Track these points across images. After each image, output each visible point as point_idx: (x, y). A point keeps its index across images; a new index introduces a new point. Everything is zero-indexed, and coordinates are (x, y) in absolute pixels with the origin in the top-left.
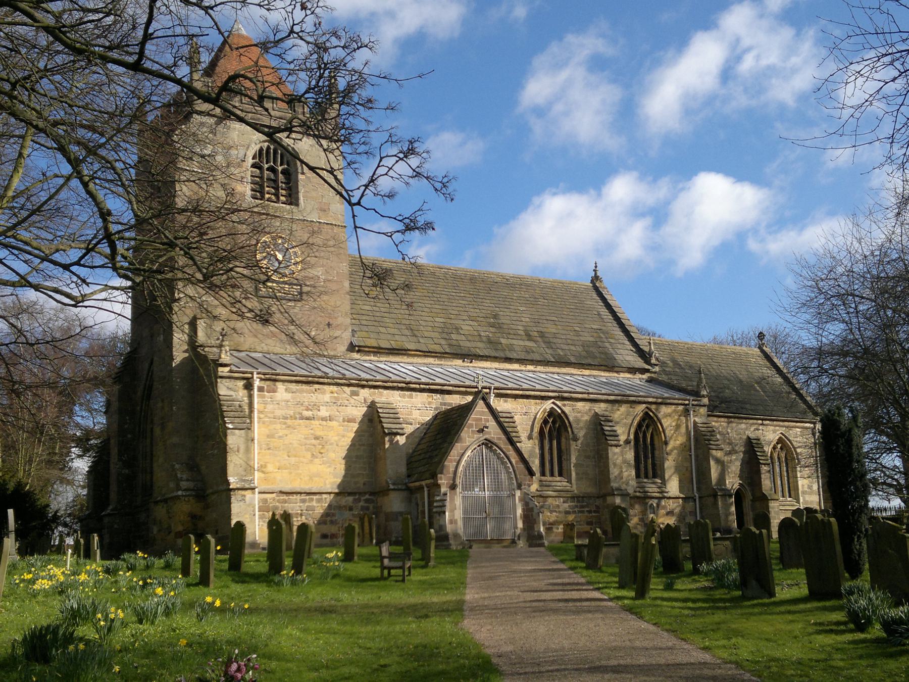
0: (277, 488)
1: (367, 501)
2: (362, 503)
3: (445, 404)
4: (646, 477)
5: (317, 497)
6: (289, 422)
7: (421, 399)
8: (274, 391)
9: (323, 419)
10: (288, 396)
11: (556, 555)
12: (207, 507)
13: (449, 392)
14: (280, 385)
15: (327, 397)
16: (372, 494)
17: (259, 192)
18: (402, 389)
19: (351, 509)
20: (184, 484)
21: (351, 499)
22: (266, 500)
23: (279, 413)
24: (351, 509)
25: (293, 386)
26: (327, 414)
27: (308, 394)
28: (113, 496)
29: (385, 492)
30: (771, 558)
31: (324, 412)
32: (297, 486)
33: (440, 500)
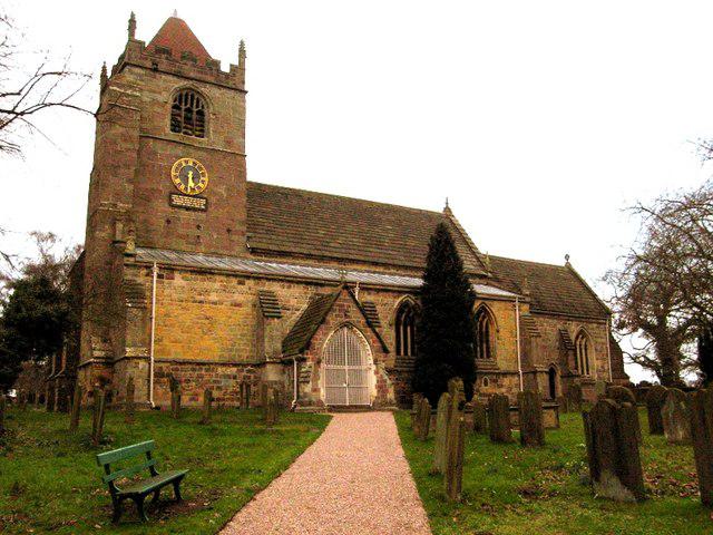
0: (171, 358)
1: (249, 371)
2: (245, 373)
3: (318, 295)
4: (482, 357)
5: (207, 367)
6: (184, 304)
7: (297, 290)
8: (173, 279)
9: (215, 303)
10: (184, 283)
11: (120, 316)
12: (113, 372)
13: (322, 285)
14: (177, 274)
15: (217, 285)
16: (253, 366)
17: (175, 127)
18: (282, 281)
19: (235, 378)
20: (96, 353)
21: (235, 369)
22: (161, 368)
23: (175, 296)
24: (235, 378)
25: (189, 275)
26: (216, 299)
27: (201, 283)
28: (64, 365)
29: (262, 364)
30: (478, 391)
31: (213, 297)
32: (189, 357)
33: (307, 372)
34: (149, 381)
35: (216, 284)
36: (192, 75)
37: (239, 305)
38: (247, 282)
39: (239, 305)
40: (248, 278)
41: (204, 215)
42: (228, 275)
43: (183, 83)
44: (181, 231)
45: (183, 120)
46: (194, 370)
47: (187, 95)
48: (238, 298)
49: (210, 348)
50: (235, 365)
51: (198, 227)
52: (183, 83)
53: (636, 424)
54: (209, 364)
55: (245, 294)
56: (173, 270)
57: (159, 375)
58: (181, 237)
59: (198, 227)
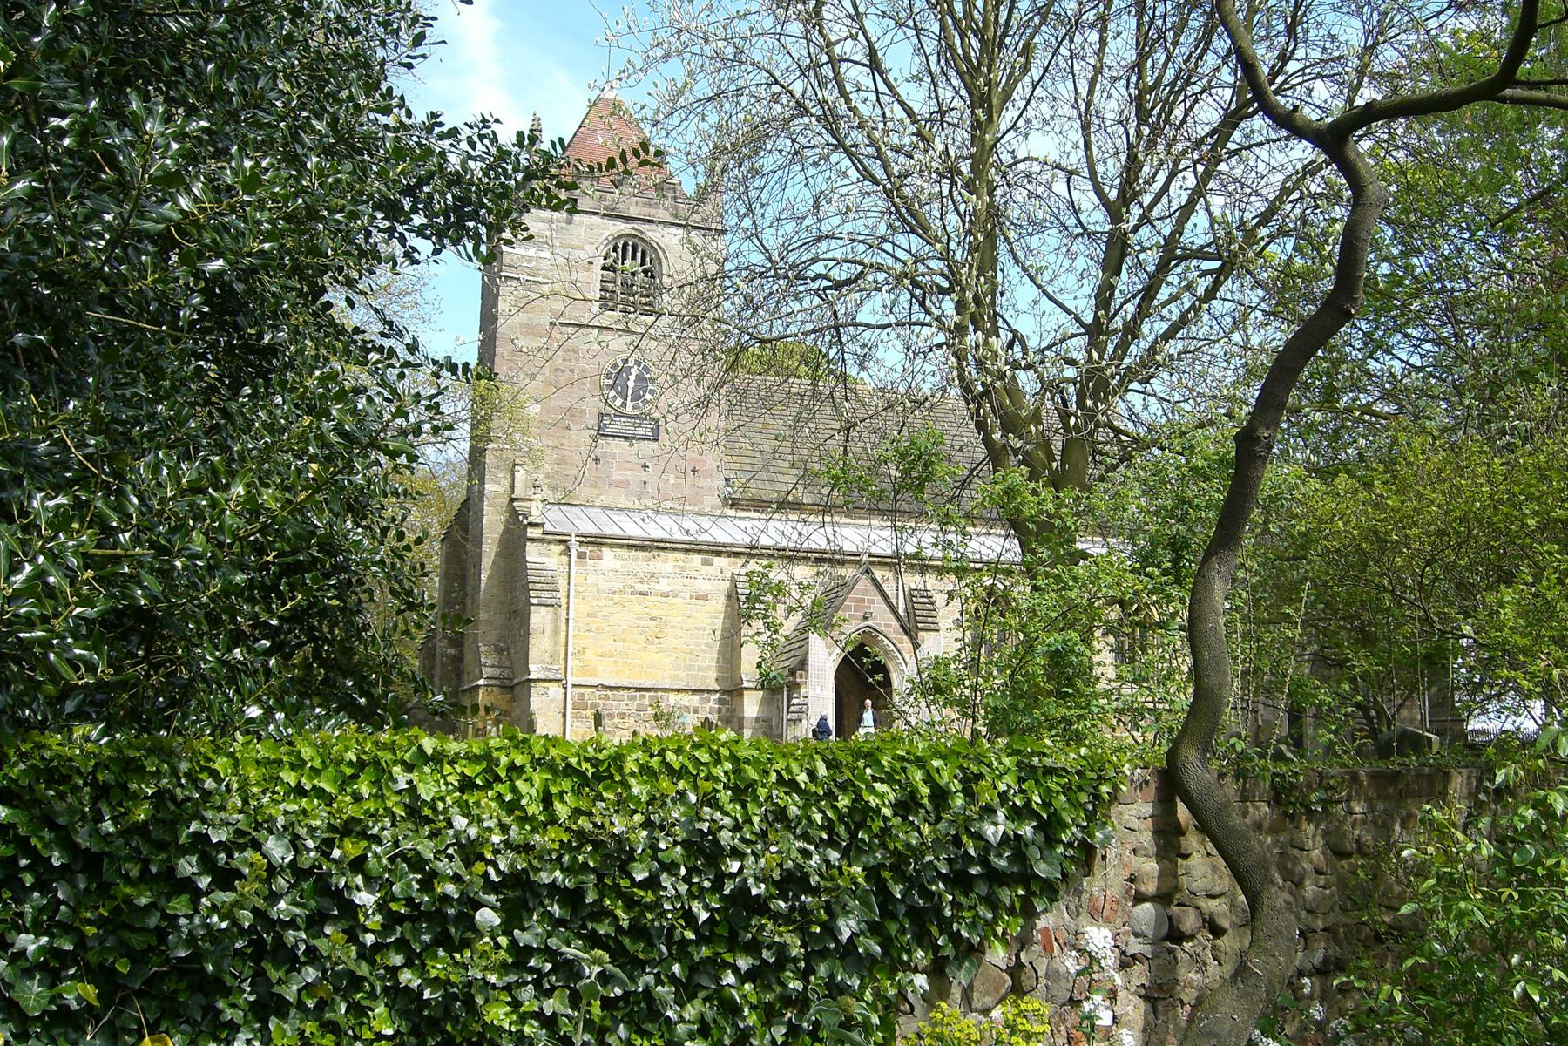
6: (616, 597)
8: (599, 558)
10: (618, 564)
13: (842, 563)
17: (607, 303)
19: (696, 711)
21: (696, 697)
23: (603, 586)
25: (624, 552)
31: (664, 586)
34: (564, 715)
35: (667, 563)
36: (634, 212)
37: (704, 597)
38: (717, 560)
39: (704, 597)
40: (719, 554)
41: (654, 445)
42: (687, 551)
43: (625, 227)
44: (617, 474)
45: (618, 289)
46: (632, 698)
47: (625, 245)
48: (703, 586)
49: (658, 667)
50: (694, 692)
51: (645, 467)
52: (625, 227)
53: (489, 578)
54: (656, 690)
55: (715, 577)
56: (602, 544)
57: (581, 706)
58: (617, 484)
59: (645, 467)
